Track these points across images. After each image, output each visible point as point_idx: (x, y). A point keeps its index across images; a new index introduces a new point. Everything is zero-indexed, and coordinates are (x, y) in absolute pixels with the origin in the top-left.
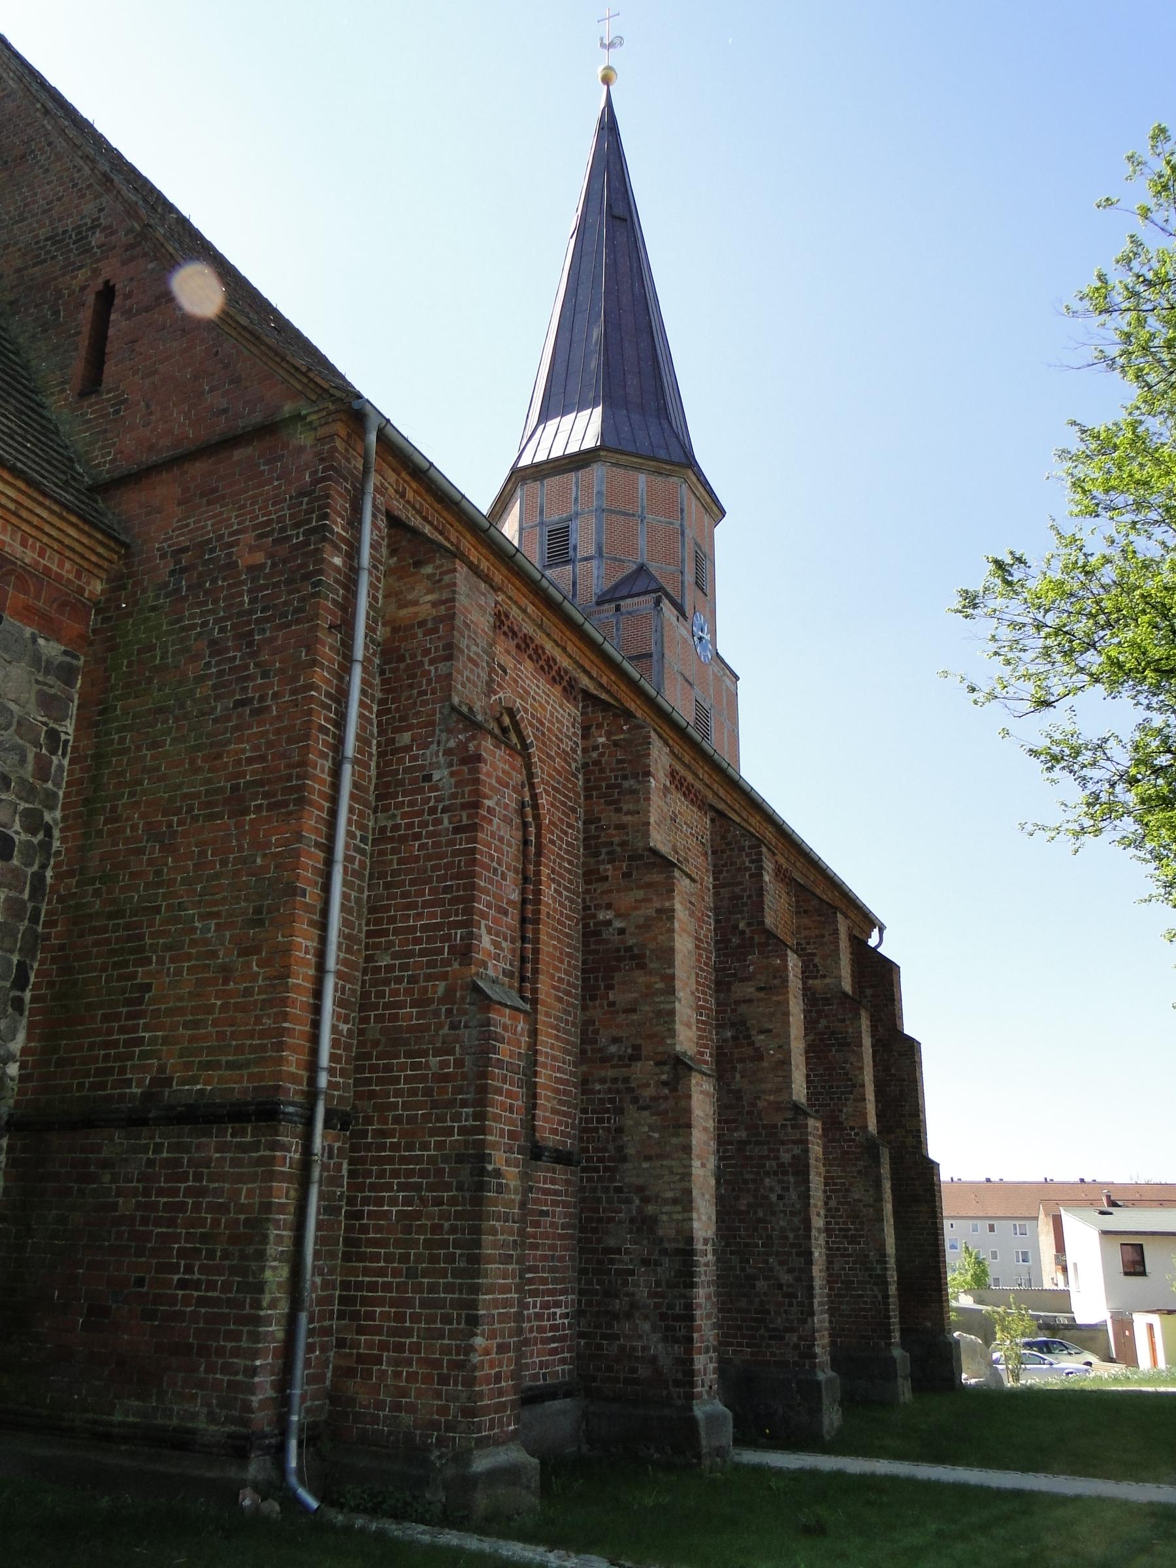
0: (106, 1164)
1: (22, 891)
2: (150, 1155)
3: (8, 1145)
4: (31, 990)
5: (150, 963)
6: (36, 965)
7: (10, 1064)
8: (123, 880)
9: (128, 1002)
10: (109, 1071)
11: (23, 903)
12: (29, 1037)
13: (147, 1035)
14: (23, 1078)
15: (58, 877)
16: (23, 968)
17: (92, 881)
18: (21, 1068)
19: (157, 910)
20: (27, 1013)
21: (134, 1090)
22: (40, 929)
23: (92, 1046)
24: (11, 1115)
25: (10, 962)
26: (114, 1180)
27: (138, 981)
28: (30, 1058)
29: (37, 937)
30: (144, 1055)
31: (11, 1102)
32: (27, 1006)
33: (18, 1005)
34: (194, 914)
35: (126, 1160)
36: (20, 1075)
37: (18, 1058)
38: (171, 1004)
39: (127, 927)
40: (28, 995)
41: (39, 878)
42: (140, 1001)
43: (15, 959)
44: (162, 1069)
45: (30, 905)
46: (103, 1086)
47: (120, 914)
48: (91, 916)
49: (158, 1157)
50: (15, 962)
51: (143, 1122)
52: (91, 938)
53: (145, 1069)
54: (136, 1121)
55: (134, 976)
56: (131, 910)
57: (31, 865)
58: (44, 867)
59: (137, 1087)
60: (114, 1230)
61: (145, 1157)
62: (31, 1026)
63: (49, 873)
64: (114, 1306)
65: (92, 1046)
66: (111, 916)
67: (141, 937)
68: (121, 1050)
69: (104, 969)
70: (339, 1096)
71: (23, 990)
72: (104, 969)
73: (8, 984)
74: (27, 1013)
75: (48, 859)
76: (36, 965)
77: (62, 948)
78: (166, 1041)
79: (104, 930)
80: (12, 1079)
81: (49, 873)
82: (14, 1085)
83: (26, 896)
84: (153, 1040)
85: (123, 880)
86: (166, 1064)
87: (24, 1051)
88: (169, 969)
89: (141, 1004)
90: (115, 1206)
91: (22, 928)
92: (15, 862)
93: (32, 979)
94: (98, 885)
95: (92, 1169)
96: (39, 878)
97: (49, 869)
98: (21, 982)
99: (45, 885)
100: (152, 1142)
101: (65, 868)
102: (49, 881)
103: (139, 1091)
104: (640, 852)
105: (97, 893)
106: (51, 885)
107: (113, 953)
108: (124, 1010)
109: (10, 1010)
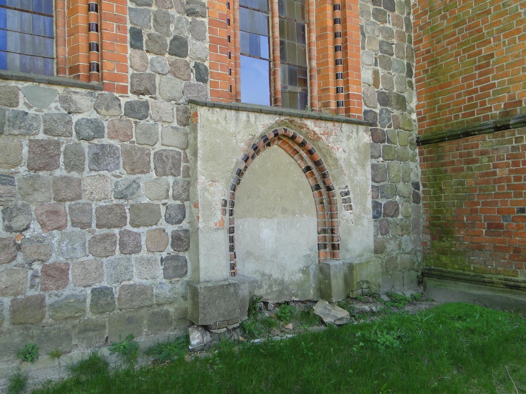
0: (483, 153)
1: (402, 28)
2: (514, 144)
3: (419, 152)
4: (415, 77)
5: (490, 42)
6: (414, 64)
7: (412, 114)
8: (460, 5)
9: (479, 67)
10: (475, 106)
11: (404, 33)
12: (419, 100)
13: (496, 82)
14: (420, 120)
15: (417, 17)
16: (409, 66)
17: (439, 12)
18: (417, 115)
19: (489, 12)
20: (415, 88)
21: (494, 112)
22: (413, 46)
23: (459, 96)
24: (418, 138)
25: (403, 64)
26: (490, 160)
27: (483, 54)
28: (422, 110)
29: (412, 50)
30: (495, 93)
31: (416, 132)
32: (414, 85)
33: (410, 84)
34: (517, 6)
35: (497, 149)
36: (418, 119)
37: (415, 110)
38: (511, 61)
39: (469, 28)
40: (413, 80)
41: (408, 19)
42: (488, 64)
43: (405, 62)
44: (512, 97)
45: (407, 34)
46: (473, 114)
47: (464, 22)
48: (442, 30)
49: (520, 144)
50: (406, 63)
51: (506, 127)
52: (445, 42)
53: (499, 100)
54: (500, 127)
55: (480, 52)
56: (469, 19)
57: (403, 14)
58: (409, 14)
59: (495, 110)
60: (496, 185)
61: (510, 146)
62: (419, 94)
63: (412, 17)
64: (505, 223)
65: (459, 96)
66: (455, 26)
67: (480, 31)
68: (480, 93)
69: (458, 54)
70: (480, 209)
71: (411, 77)
72: (458, 54)
73: (405, 75)
74: (415, 88)
75: (410, 10)
76: (414, 64)
77: (428, 52)
78: (510, 82)
79: (454, 34)
80: (415, 121)
81: (412, 17)
82: (416, 124)
83: (404, 30)
84: (502, 83)
85: (460, 5)
86: (514, 95)
87: (417, 107)
88: (504, 42)
89: (488, 66)
90: (495, 173)
91: (405, 46)
92: (397, 12)
93: (414, 72)
94: (443, 13)
95: (474, 157)
96: (408, 19)
97: (411, 14)
98: (410, 74)
99: (411, 24)
100: (514, 137)
101: (420, 12)
102: (412, 21)
103: (498, 112)
104: (474, 186)
105: (444, 17)
106: (414, 23)
107: (463, 44)
108: (477, 72)
109: (408, 88)
